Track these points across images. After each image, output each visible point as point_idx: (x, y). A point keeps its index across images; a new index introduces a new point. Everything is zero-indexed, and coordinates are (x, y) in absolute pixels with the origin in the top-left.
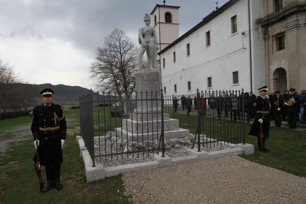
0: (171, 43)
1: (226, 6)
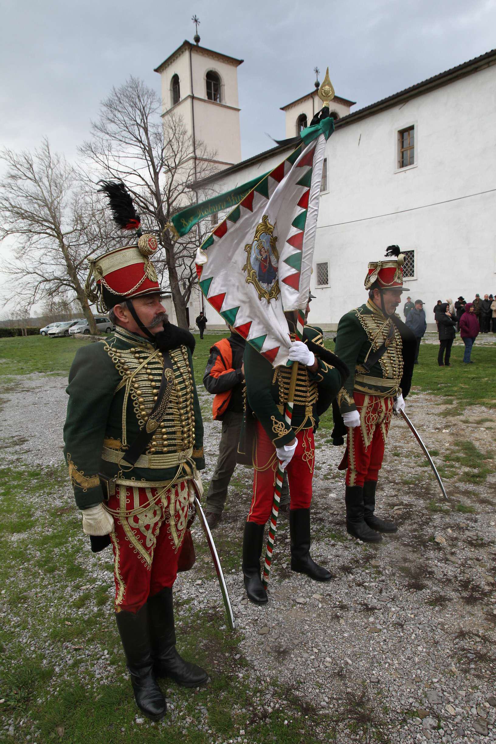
0: (236, 162)
1: (491, 59)
